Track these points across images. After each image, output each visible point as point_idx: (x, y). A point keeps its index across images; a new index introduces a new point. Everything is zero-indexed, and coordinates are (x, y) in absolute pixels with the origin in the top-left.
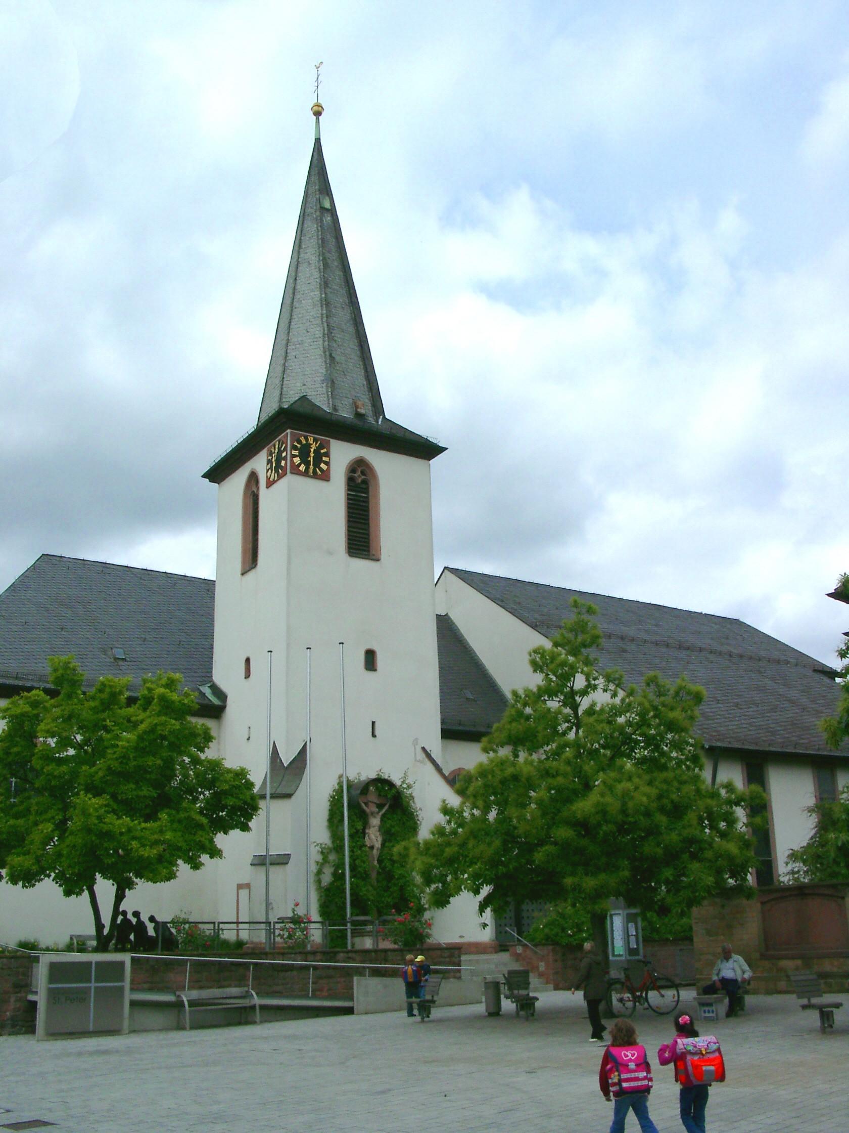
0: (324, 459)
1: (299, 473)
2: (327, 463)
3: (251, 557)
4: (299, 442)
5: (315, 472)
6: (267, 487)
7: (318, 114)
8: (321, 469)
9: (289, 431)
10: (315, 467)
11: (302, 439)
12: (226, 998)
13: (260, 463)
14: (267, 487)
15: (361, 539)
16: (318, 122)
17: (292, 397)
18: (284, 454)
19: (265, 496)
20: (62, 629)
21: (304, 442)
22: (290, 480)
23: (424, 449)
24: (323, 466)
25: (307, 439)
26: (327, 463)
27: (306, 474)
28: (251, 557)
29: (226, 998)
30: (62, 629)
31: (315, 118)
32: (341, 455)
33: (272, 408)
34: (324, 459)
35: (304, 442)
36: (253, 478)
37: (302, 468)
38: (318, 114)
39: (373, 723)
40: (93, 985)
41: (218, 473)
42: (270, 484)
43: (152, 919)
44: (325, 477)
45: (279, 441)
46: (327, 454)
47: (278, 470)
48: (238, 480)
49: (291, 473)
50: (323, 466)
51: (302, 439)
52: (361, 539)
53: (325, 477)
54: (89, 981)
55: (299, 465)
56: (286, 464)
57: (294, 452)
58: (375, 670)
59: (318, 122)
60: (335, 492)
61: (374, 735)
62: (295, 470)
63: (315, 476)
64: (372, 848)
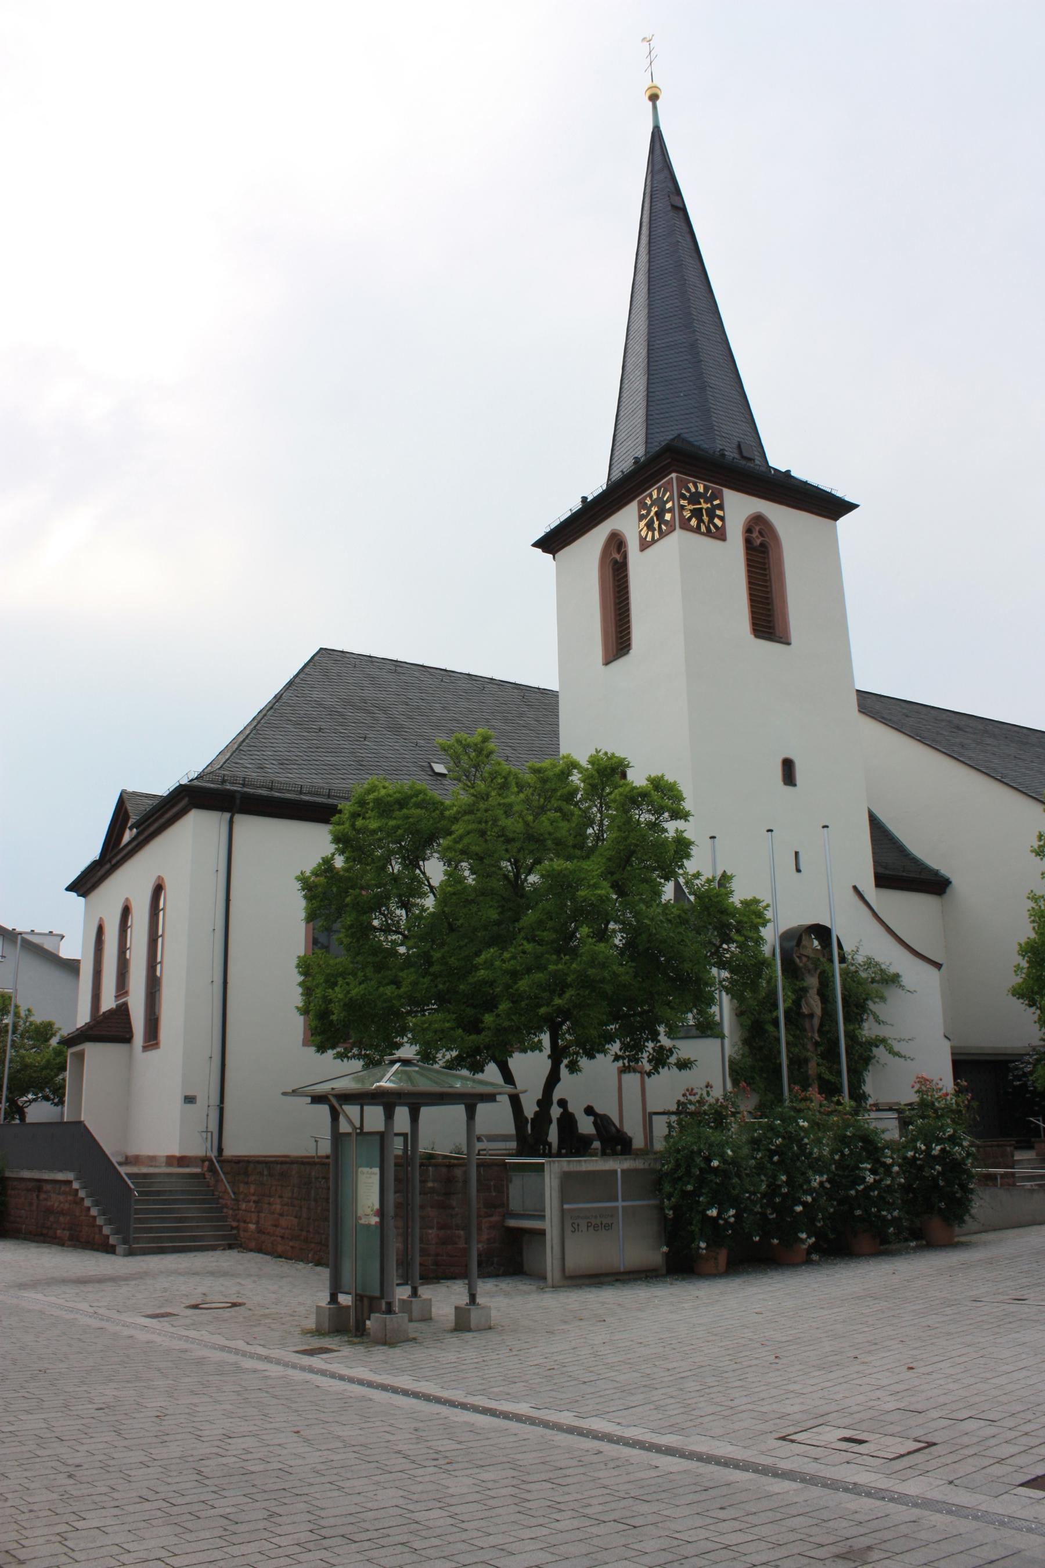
0: (718, 512)
1: (690, 529)
2: (722, 518)
3: (618, 640)
4: (688, 490)
5: (708, 529)
6: (642, 550)
7: (654, 98)
8: (715, 526)
9: (674, 475)
10: (707, 523)
11: (691, 485)
12: (100, 1280)
13: (627, 521)
14: (642, 550)
15: (767, 619)
16: (655, 108)
17: (665, 437)
18: (669, 505)
19: (637, 562)
20: (365, 738)
21: (693, 490)
22: (678, 538)
23: (831, 507)
24: (717, 521)
25: (696, 488)
26: (722, 518)
27: (697, 530)
28: (618, 640)
29: (100, 1280)
30: (365, 738)
31: (650, 104)
32: (738, 507)
33: (636, 449)
34: (718, 512)
35: (693, 490)
36: (616, 543)
37: (694, 522)
38: (654, 98)
39: (797, 853)
40: (620, 1204)
41: (552, 542)
42: (644, 545)
43: (589, 1111)
44: (720, 535)
45: (659, 489)
46: (721, 507)
47: (658, 526)
48: (594, 541)
49: (681, 528)
50: (717, 521)
51: (691, 485)
52: (767, 619)
53: (720, 535)
54: (617, 1200)
55: (690, 519)
56: (673, 517)
57: (683, 502)
58: (795, 785)
59: (655, 108)
60: (733, 553)
61: (798, 870)
62: (685, 525)
63: (709, 533)
64: (811, 1016)
